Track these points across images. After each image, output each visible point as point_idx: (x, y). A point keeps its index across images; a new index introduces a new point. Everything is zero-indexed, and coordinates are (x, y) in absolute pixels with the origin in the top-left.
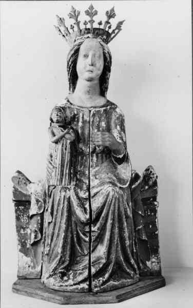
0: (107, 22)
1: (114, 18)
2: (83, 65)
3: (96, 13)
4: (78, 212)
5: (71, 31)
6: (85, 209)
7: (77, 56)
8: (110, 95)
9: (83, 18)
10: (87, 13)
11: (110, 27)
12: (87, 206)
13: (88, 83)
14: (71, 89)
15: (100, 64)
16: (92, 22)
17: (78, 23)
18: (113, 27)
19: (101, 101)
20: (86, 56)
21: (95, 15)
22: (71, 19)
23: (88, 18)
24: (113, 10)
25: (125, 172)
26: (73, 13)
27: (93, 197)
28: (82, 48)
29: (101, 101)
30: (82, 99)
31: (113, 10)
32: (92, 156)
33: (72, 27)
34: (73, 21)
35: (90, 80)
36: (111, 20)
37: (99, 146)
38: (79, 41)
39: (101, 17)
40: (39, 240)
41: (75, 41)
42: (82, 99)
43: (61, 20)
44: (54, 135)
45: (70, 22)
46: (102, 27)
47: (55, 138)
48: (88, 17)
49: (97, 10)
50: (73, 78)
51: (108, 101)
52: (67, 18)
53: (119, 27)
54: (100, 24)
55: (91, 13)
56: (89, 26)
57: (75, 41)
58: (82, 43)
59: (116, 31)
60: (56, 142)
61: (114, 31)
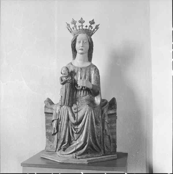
0: (90, 26)
1: (94, 24)
2: (78, 46)
3: (84, 22)
4: (72, 118)
5: (73, 30)
6: (75, 117)
7: (76, 42)
8: (94, 61)
9: (78, 24)
10: (80, 22)
11: (92, 28)
12: (76, 116)
13: (81, 55)
14: (74, 57)
15: (87, 46)
16: (82, 26)
17: (76, 27)
18: (94, 28)
19: (88, 64)
20: (80, 42)
21: (83, 22)
22: (72, 25)
23: (80, 24)
24: (93, 20)
25: (97, 100)
26: (81, 21)
27: (79, 111)
28: (78, 38)
29: (88, 64)
30: (79, 62)
31: (93, 20)
32: (81, 92)
33: (73, 29)
34: (73, 25)
35: (81, 54)
36: (92, 25)
37: (84, 87)
38: (76, 35)
39: (87, 24)
40: (102, 114)
41: (75, 35)
42: (79, 62)
43: (68, 25)
44: (62, 80)
45: (72, 26)
46: (87, 28)
47: (62, 82)
48: (89, 24)
49: (84, 20)
50: (74, 51)
51: (92, 64)
52: (70, 24)
53: (97, 27)
54: (86, 26)
55: (82, 22)
56: (81, 28)
57: (75, 35)
58: (78, 35)
59: (96, 30)
60: (63, 84)
61: (94, 29)
